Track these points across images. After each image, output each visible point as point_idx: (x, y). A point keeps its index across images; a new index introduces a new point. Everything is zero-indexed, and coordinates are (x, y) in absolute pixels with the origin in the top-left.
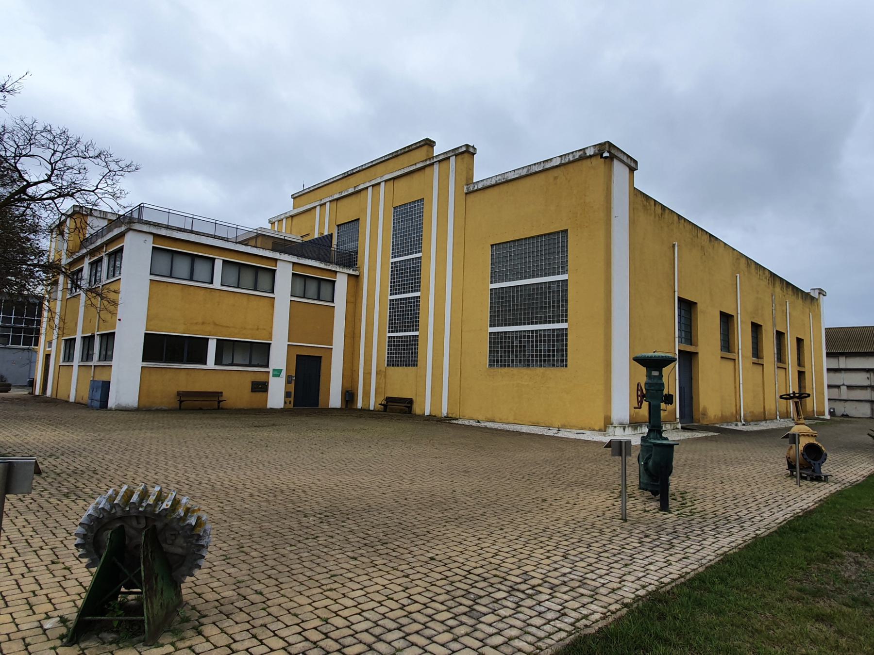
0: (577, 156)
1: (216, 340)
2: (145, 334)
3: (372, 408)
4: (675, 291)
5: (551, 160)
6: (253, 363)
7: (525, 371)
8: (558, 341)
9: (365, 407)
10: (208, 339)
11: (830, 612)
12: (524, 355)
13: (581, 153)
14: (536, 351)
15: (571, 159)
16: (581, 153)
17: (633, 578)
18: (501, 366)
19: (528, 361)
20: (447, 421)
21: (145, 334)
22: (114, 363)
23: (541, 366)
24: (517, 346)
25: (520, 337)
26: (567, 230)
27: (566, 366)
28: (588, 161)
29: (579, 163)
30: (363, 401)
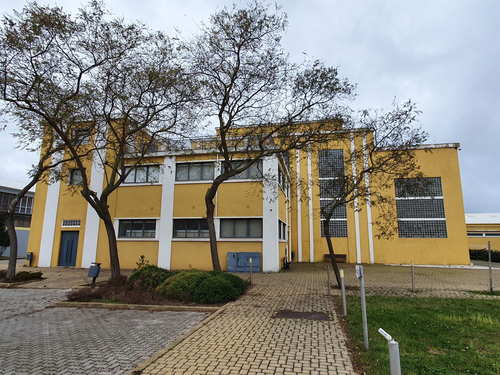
0: (444, 146)
1: (118, 220)
2: (174, 220)
3: (312, 260)
4: (146, 185)
5: (429, 145)
6: (136, 236)
7: (422, 239)
8: (430, 226)
9: (307, 260)
10: (155, 220)
11: (476, 316)
12: (421, 232)
13: (446, 145)
14: (428, 230)
15: (441, 147)
16: (446, 145)
17: (212, 350)
18: (407, 237)
19: (424, 235)
20: (376, 265)
21: (174, 220)
22: (264, 239)
23: (431, 237)
24: (416, 228)
25: (418, 224)
26: (440, 177)
27: (446, 237)
28: (449, 149)
29: (445, 149)
30: (302, 257)
